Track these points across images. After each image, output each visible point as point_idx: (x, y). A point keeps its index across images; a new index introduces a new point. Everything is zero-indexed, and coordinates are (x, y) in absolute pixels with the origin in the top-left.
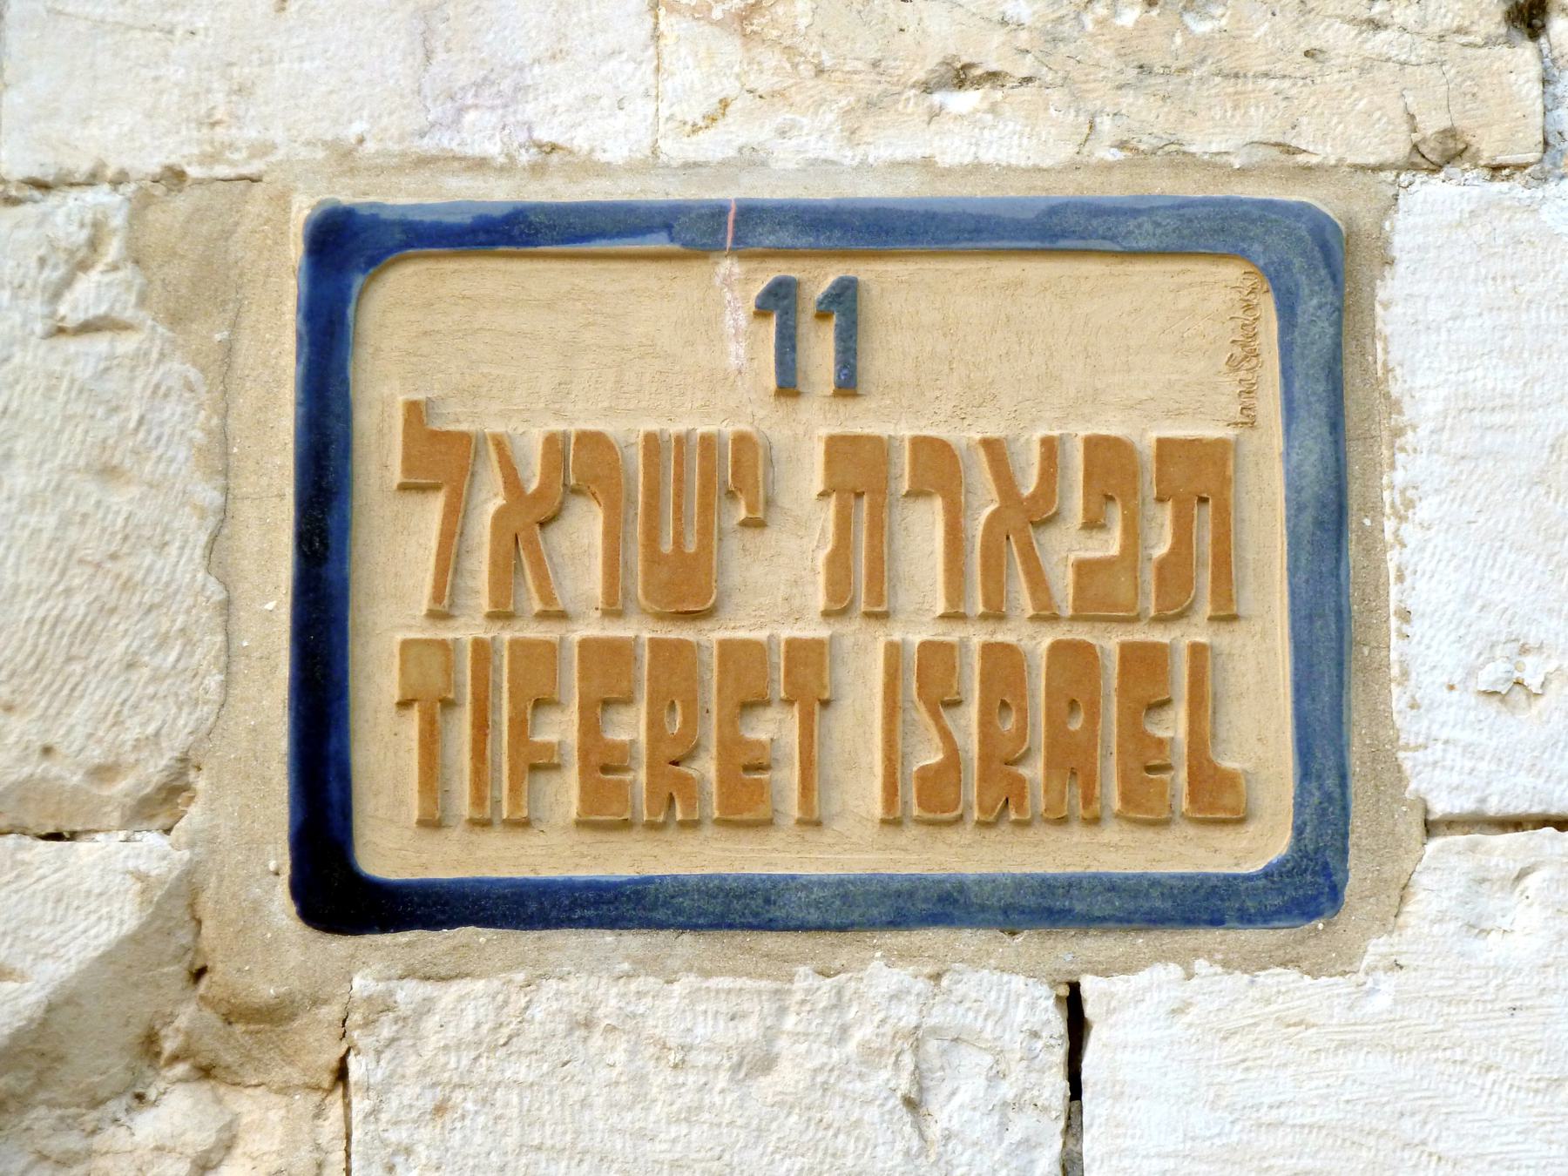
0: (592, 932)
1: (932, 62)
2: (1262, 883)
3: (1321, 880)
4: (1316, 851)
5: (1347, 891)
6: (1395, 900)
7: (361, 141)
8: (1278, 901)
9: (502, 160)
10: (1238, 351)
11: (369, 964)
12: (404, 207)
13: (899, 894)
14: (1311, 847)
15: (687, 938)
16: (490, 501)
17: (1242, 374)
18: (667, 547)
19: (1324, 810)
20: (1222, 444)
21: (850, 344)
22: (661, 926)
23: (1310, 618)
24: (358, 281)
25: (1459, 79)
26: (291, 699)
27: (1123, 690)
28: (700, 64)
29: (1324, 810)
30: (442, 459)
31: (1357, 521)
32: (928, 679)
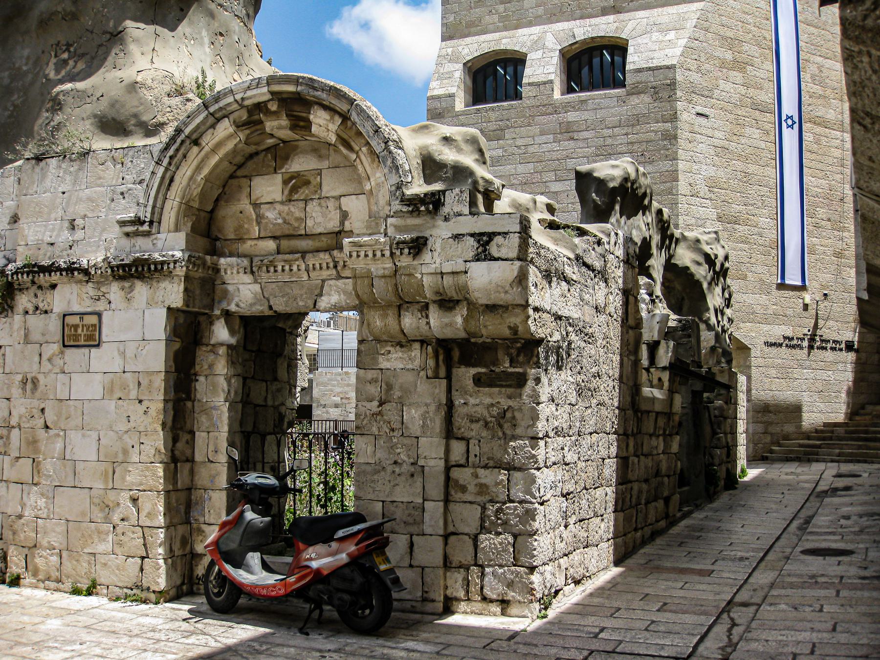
11: (65, 349)
28: (78, 306)
30: (68, 325)
32: (85, 335)
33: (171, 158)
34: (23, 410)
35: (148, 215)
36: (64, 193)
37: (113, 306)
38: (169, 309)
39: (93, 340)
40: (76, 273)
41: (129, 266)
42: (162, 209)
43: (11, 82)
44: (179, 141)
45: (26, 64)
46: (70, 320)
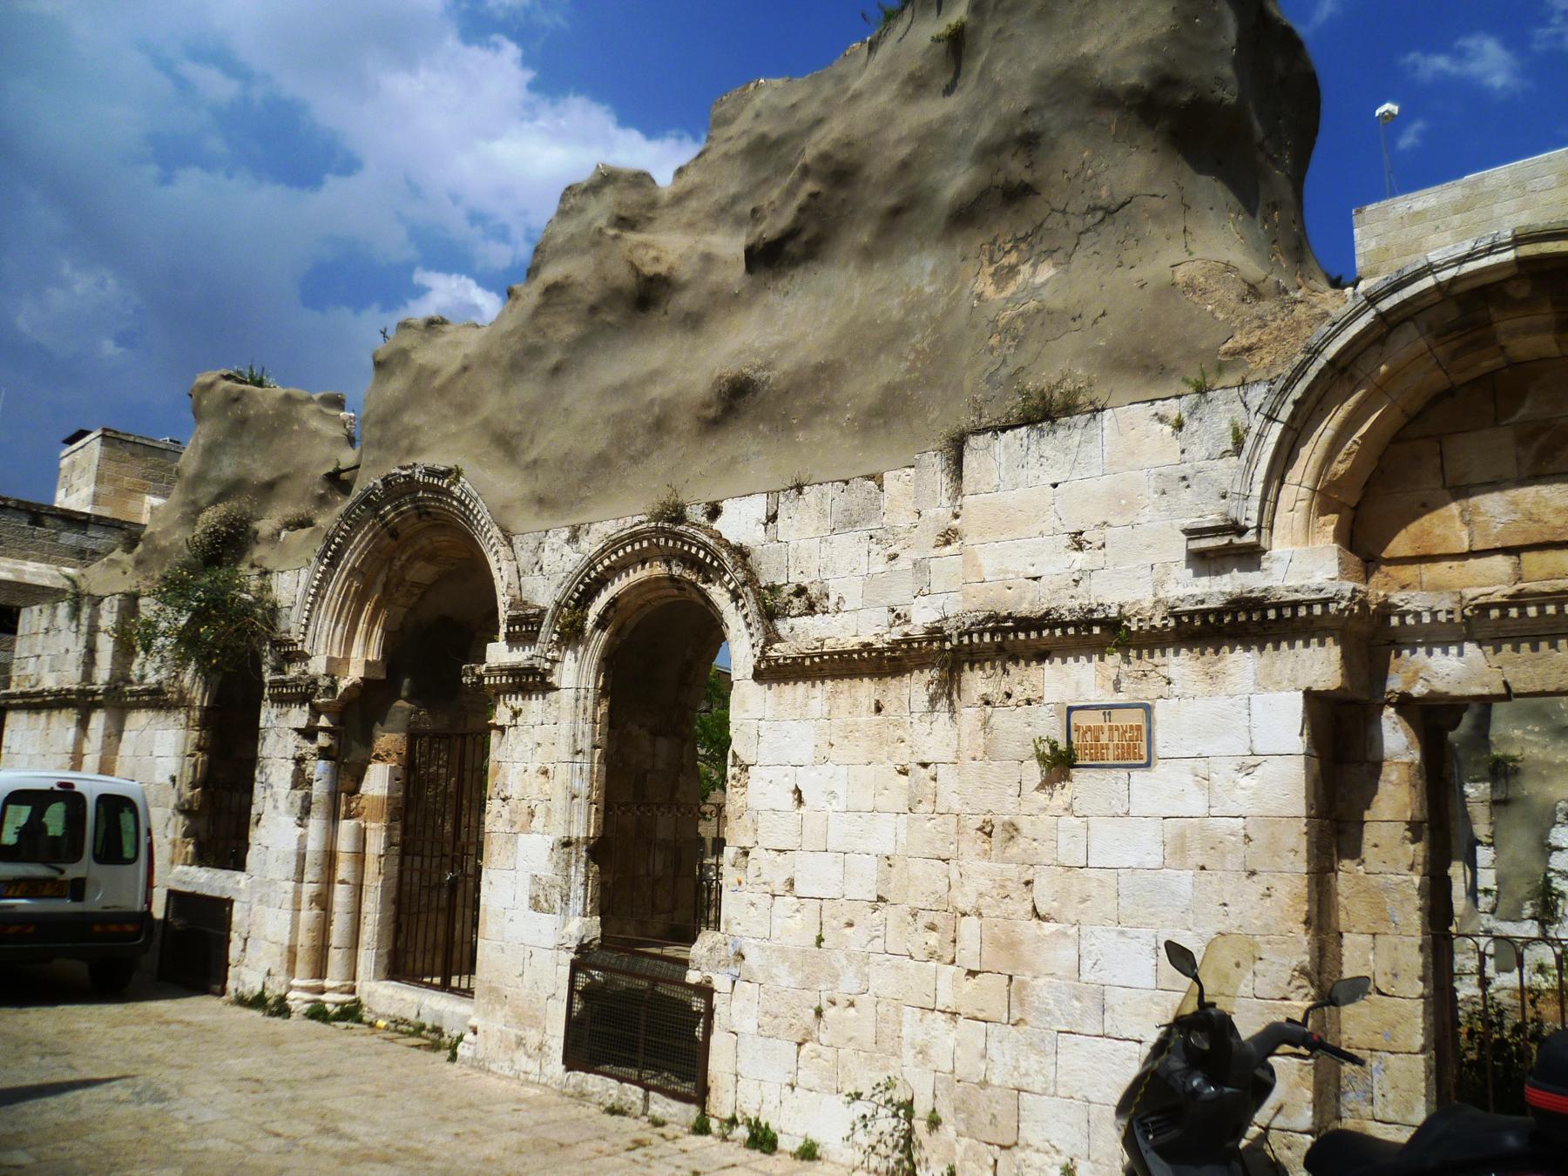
33: (1296, 403)
34: (985, 884)
35: (1254, 515)
36: (1055, 486)
37: (1176, 688)
38: (1309, 695)
39: (1137, 753)
40: (1096, 630)
41: (1219, 612)
42: (1276, 503)
43: (907, 314)
44: (1313, 372)
45: (931, 283)
46: (1078, 719)
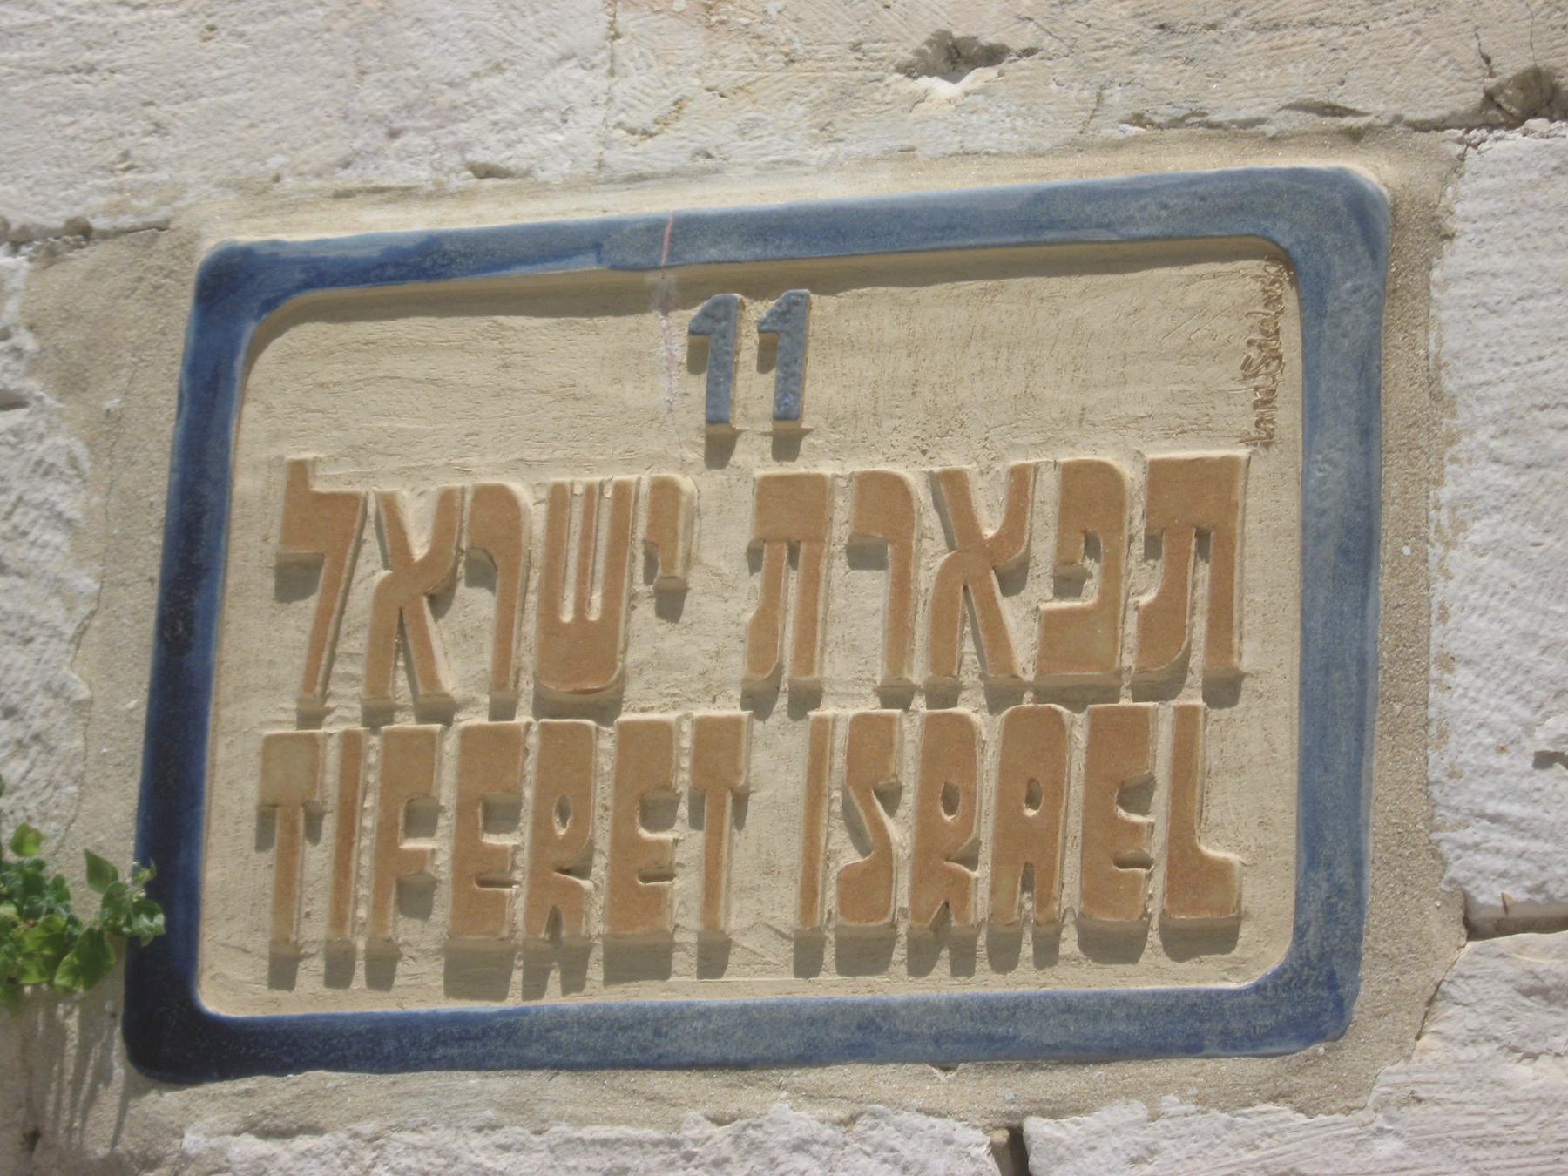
0: (455, 1074)
1: (918, 42)
2: (1250, 999)
3: (1324, 994)
4: (1321, 957)
5: (1356, 1007)
6: (1416, 1018)
7: (277, 179)
8: (1270, 1021)
9: (430, 187)
10: (1253, 353)
12: (307, 243)
13: (812, 1021)
14: (1314, 953)
15: (563, 1078)
16: (371, 573)
17: (1260, 381)
18: (567, 617)
19: (1332, 906)
20: (1230, 464)
21: (795, 368)
22: (534, 1065)
23: (1326, 670)
24: (250, 329)
25: (1547, 10)
26: (140, 809)
27: (1092, 766)
29: (1332, 906)
31: (1393, 546)
